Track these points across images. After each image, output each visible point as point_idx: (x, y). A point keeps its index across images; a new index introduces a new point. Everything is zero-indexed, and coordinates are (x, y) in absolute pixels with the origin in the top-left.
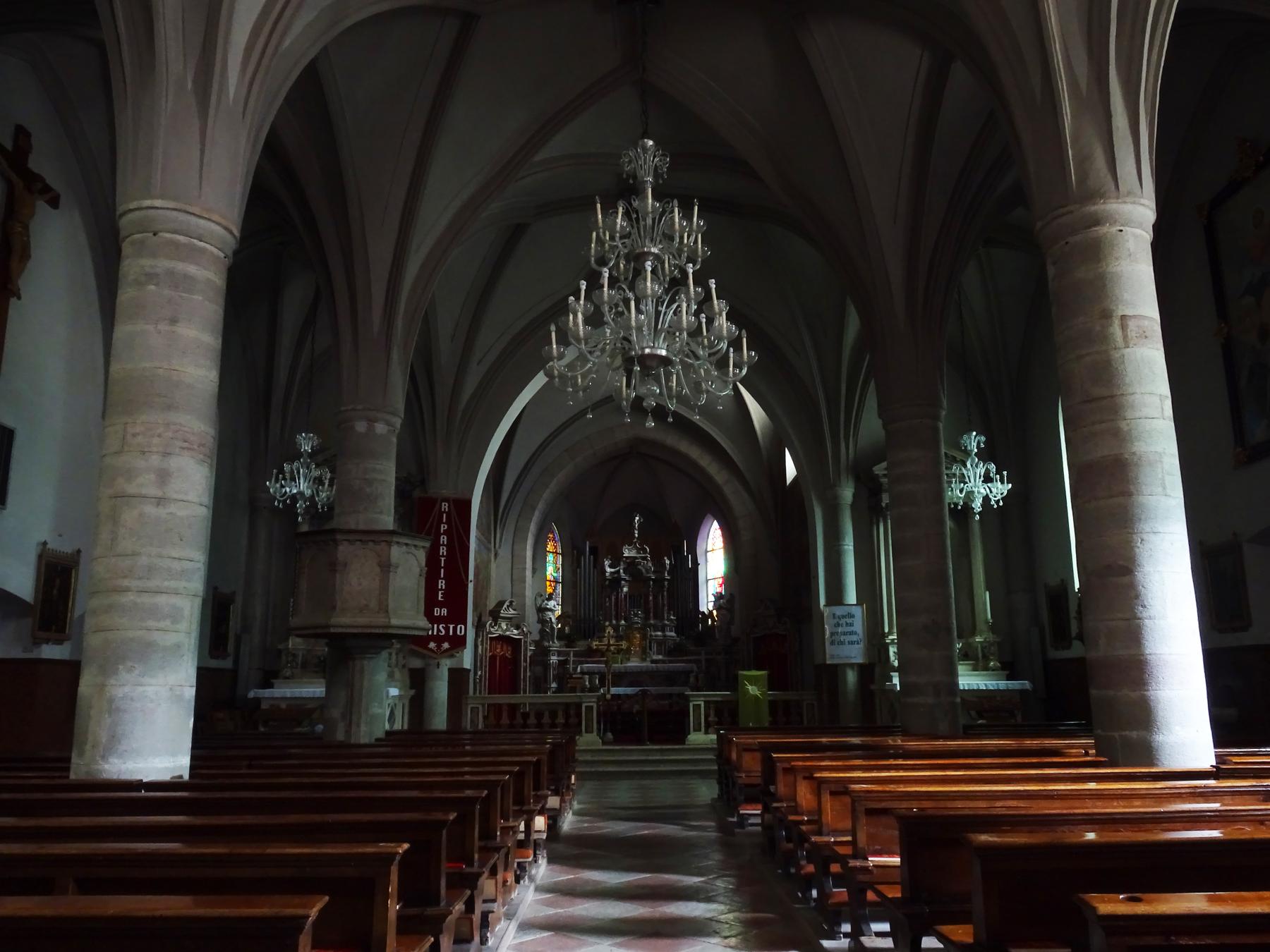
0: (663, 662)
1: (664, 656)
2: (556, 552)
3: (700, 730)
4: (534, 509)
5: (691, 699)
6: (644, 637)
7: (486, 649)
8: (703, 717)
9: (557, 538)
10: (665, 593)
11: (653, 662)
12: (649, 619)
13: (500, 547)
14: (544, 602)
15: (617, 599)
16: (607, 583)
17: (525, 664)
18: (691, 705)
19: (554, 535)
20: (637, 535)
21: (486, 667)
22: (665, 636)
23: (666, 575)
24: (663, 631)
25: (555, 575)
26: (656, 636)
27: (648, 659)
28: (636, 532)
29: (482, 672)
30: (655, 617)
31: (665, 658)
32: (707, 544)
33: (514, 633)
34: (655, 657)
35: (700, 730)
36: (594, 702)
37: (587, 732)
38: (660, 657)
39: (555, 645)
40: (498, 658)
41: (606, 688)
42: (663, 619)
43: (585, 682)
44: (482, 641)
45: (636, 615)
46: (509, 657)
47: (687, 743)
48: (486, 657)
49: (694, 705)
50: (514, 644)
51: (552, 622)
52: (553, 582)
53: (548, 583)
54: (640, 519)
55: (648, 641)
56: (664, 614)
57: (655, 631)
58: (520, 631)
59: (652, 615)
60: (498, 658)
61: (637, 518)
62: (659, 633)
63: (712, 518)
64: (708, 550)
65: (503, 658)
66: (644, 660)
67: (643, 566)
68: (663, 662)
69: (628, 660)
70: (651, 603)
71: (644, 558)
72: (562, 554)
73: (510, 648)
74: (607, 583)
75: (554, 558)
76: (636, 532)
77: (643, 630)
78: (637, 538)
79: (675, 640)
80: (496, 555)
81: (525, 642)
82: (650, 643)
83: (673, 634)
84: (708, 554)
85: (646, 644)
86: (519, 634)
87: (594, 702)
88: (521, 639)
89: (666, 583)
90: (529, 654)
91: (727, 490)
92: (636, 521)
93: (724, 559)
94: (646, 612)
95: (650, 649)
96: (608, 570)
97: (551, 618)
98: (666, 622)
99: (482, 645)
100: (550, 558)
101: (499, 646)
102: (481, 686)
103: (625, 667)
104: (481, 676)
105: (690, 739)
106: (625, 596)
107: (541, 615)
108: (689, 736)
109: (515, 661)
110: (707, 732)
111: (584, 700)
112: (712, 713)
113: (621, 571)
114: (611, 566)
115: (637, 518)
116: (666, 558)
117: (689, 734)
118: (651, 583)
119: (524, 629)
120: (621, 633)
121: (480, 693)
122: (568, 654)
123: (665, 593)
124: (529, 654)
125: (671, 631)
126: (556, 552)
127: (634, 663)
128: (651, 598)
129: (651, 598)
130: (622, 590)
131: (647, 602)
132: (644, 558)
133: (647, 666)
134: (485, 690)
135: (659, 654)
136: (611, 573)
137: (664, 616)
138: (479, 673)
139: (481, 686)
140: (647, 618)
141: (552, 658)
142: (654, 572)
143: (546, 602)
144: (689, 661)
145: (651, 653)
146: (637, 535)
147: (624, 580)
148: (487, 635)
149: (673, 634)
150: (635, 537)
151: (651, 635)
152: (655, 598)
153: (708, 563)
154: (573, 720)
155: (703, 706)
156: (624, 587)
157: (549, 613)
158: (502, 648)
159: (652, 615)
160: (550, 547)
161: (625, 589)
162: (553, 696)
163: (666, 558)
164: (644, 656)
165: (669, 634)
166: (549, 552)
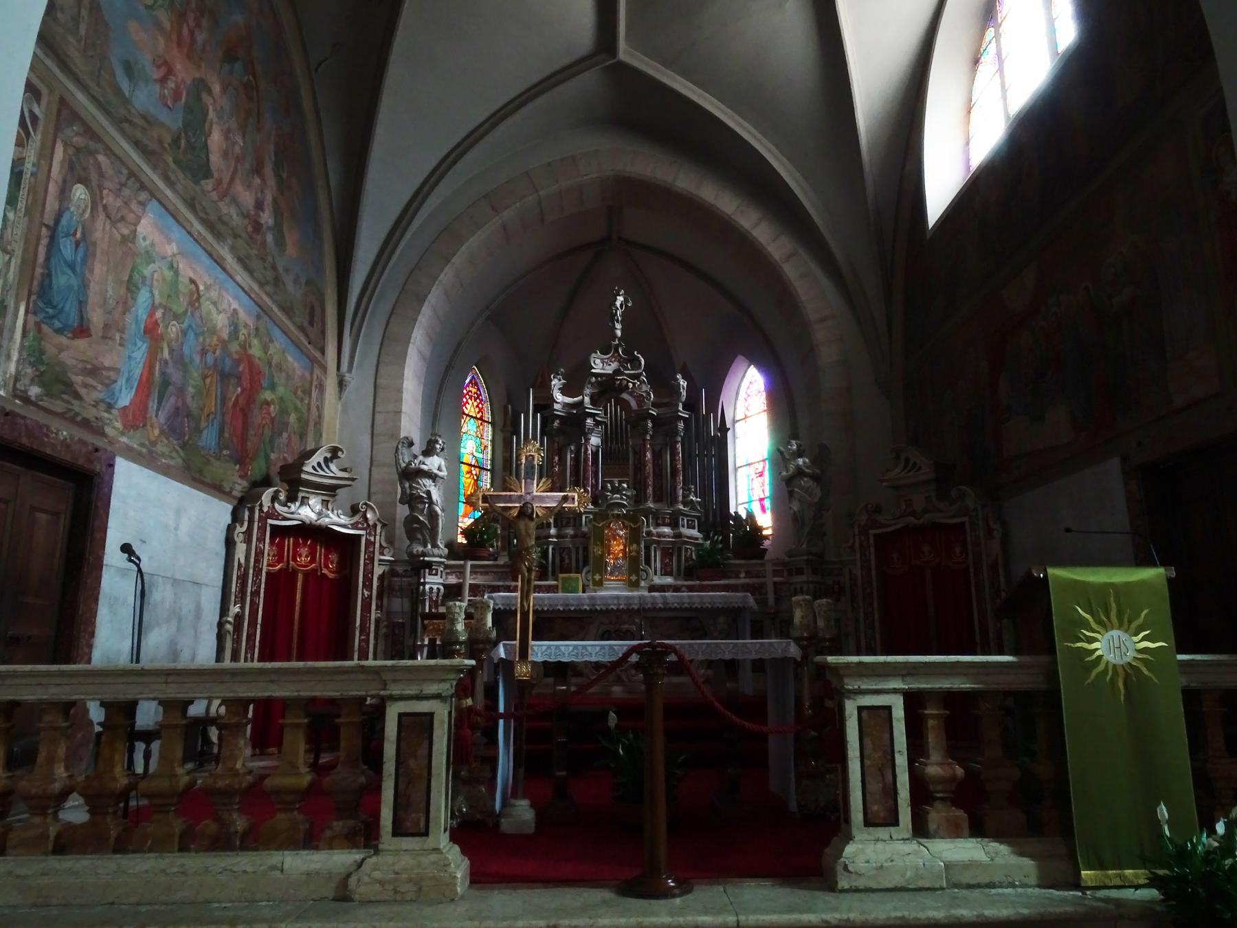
0: (676, 589)
1: (676, 579)
2: (481, 419)
3: (895, 822)
4: (421, 299)
5: (851, 684)
6: (634, 536)
7: (259, 553)
8: (901, 761)
9: (485, 395)
10: (679, 446)
11: (652, 588)
12: (646, 500)
13: (350, 369)
14: (415, 457)
15: (576, 460)
16: (556, 424)
17: (366, 593)
18: (851, 708)
19: (478, 389)
20: (619, 333)
21: (256, 593)
22: (679, 536)
23: (680, 408)
24: (674, 524)
25: (480, 456)
26: (659, 535)
27: (643, 584)
28: (618, 326)
29: (242, 608)
30: (658, 499)
31: (680, 583)
32: (735, 409)
33: (338, 521)
34: (658, 580)
35: (895, 822)
36: (437, 696)
37: (399, 830)
38: (669, 580)
39: (436, 551)
40: (300, 577)
41: (517, 643)
42: (674, 500)
43: (453, 621)
44: (248, 534)
45: (616, 490)
46: (331, 576)
47: (843, 883)
48: (258, 572)
49: (861, 709)
50: (345, 546)
51: (431, 502)
52: (474, 466)
53: (464, 468)
54: (626, 300)
55: (642, 546)
56: (675, 488)
57: (657, 525)
58: (356, 518)
59: (650, 490)
60: (300, 577)
61: (620, 299)
62: (667, 530)
63: (746, 363)
64: (737, 418)
65: (313, 578)
66: (634, 585)
67: (631, 394)
68: (676, 589)
69: (599, 584)
70: (650, 467)
71: (637, 377)
72: (493, 424)
73: (334, 557)
74: (556, 424)
75: (478, 427)
76: (618, 326)
77: (632, 520)
78: (620, 339)
79: (701, 545)
80: (341, 384)
81: (369, 544)
82: (647, 548)
83: (694, 533)
84: (737, 425)
85: (638, 552)
86: (354, 526)
87: (437, 696)
88: (360, 536)
89: (681, 425)
90: (378, 570)
91: (790, 271)
92: (618, 304)
93: (769, 426)
94: (639, 485)
95: (648, 562)
96: (559, 397)
97: (428, 493)
98: (681, 507)
99: (248, 540)
100: (469, 426)
101: (304, 551)
102: (237, 641)
103: (592, 598)
104: (239, 618)
105: (859, 865)
106: (595, 454)
107: (407, 485)
108: (849, 849)
109: (344, 586)
110: (920, 830)
111: (395, 690)
112: (934, 738)
113: (587, 399)
114: (565, 391)
115: (620, 299)
116: (679, 376)
117: (849, 838)
118: (650, 425)
119: (369, 516)
120: (585, 529)
121: (235, 657)
122: (460, 572)
123: (679, 446)
124: (378, 570)
125: (691, 527)
126: (481, 419)
127: (613, 591)
128: (649, 455)
129: (649, 455)
130: (587, 440)
131: (640, 466)
132: (637, 377)
133: (640, 598)
134: (250, 647)
135: (666, 572)
136: (566, 405)
137: (676, 497)
138: (234, 609)
139: (237, 641)
140: (639, 498)
141: (429, 579)
142: (655, 405)
143: (421, 458)
144: (733, 588)
145: (651, 572)
146: (619, 333)
147: (593, 415)
148: (263, 520)
149: (694, 533)
150: (615, 336)
151: (649, 534)
152: (657, 456)
153: (737, 441)
154: (346, 777)
155: (899, 713)
156: (591, 431)
157: (428, 482)
158: (312, 554)
159: (650, 490)
160: (470, 408)
161: (595, 440)
162: (261, 672)
163: (679, 376)
164: (634, 578)
165: (685, 531)
166: (468, 415)
